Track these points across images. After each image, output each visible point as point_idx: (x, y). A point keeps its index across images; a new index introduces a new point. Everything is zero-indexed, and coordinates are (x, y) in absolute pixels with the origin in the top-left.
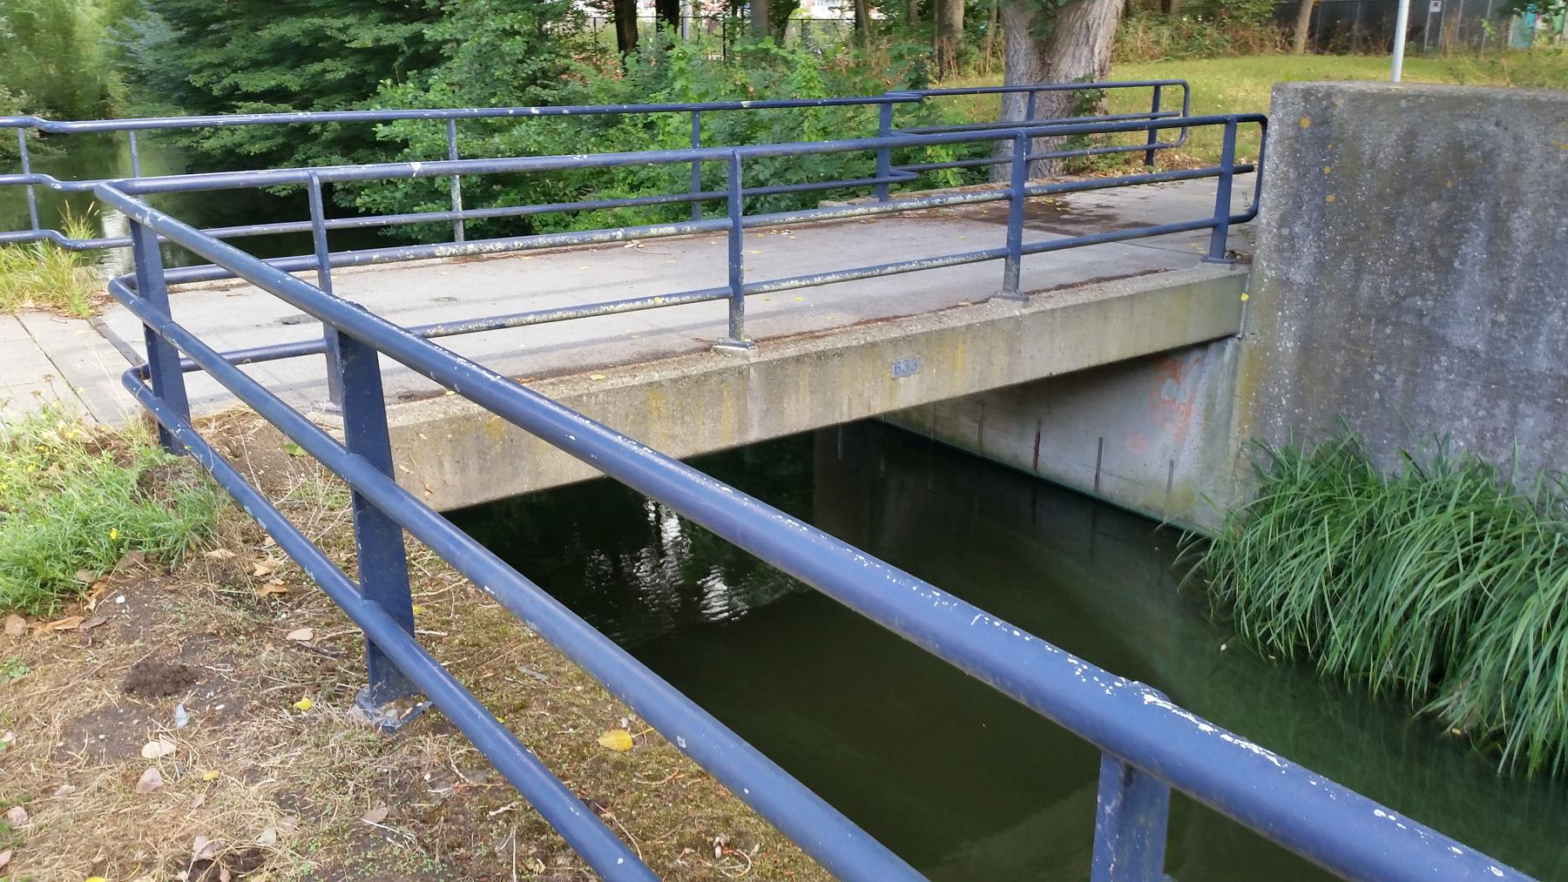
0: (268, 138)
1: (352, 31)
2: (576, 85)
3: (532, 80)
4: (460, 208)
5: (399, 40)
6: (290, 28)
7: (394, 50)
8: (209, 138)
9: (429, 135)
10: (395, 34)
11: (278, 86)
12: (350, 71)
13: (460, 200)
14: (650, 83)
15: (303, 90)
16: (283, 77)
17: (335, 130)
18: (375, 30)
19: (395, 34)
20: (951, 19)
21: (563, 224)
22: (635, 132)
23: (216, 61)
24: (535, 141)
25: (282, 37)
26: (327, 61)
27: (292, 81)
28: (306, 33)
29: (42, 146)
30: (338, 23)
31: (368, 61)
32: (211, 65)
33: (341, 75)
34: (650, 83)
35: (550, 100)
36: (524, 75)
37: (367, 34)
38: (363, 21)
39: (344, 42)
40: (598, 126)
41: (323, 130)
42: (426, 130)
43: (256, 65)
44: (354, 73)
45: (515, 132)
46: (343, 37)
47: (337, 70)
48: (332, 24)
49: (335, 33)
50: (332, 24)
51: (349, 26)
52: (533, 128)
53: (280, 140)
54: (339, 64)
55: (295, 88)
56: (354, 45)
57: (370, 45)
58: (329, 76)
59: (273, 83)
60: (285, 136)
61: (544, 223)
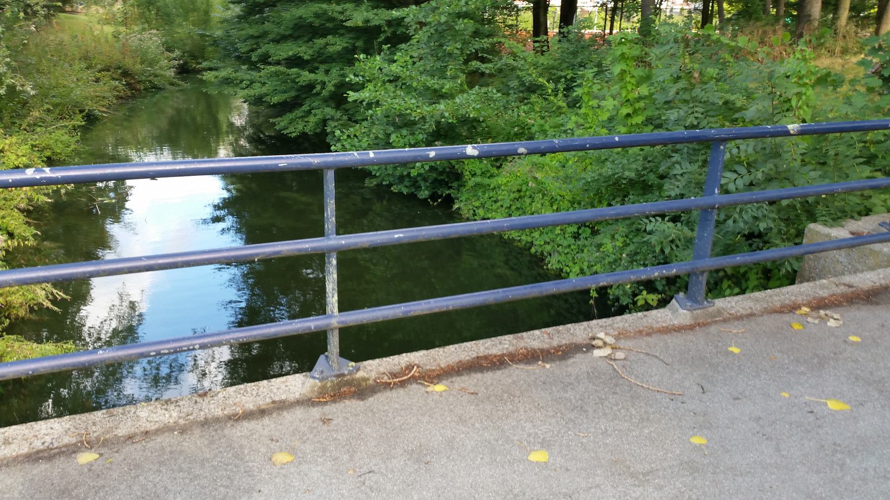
0: (285, 92)
1: (348, 13)
2: (507, 60)
3: (475, 56)
4: (336, 310)
5: (382, 22)
6: (291, 14)
7: (378, 29)
8: (244, 89)
9: (389, 100)
10: (381, 16)
11: (295, 56)
12: (345, 45)
13: (336, 297)
14: (567, 58)
15: (313, 60)
16: (300, 49)
17: (330, 91)
18: (365, 14)
19: (381, 16)
20: (810, 10)
21: (488, 175)
22: (555, 101)
23: (256, 34)
24: (473, 108)
25: (300, 18)
26: (330, 37)
27: (304, 51)
28: (317, 15)
29: (176, 80)
30: (339, 8)
31: (358, 38)
32: (252, 37)
33: (338, 48)
34: (567, 58)
35: (487, 72)
36: (469, 52)
37: (359, 16)
38: (358, 8)
39: (343, 21)
40: (522, 92)
41: (323, 88)
42: (387, 95)
43: (280, 40)
44: (347, 47)
45: (457, 100)
46: (342, 17)
47: (337, 44)
48: (333, 9)
49: (335, 15)
50: (333, 9)
51: (346, 10)
52: (472, 97)
53: (293, 94)
54: (337, 40)
55: (306, 57)
56: (348, 24)
57: (360, 24)
58: (331, 49)
59: (290, 53)
60: (298, 90)
61: (473, 173)
